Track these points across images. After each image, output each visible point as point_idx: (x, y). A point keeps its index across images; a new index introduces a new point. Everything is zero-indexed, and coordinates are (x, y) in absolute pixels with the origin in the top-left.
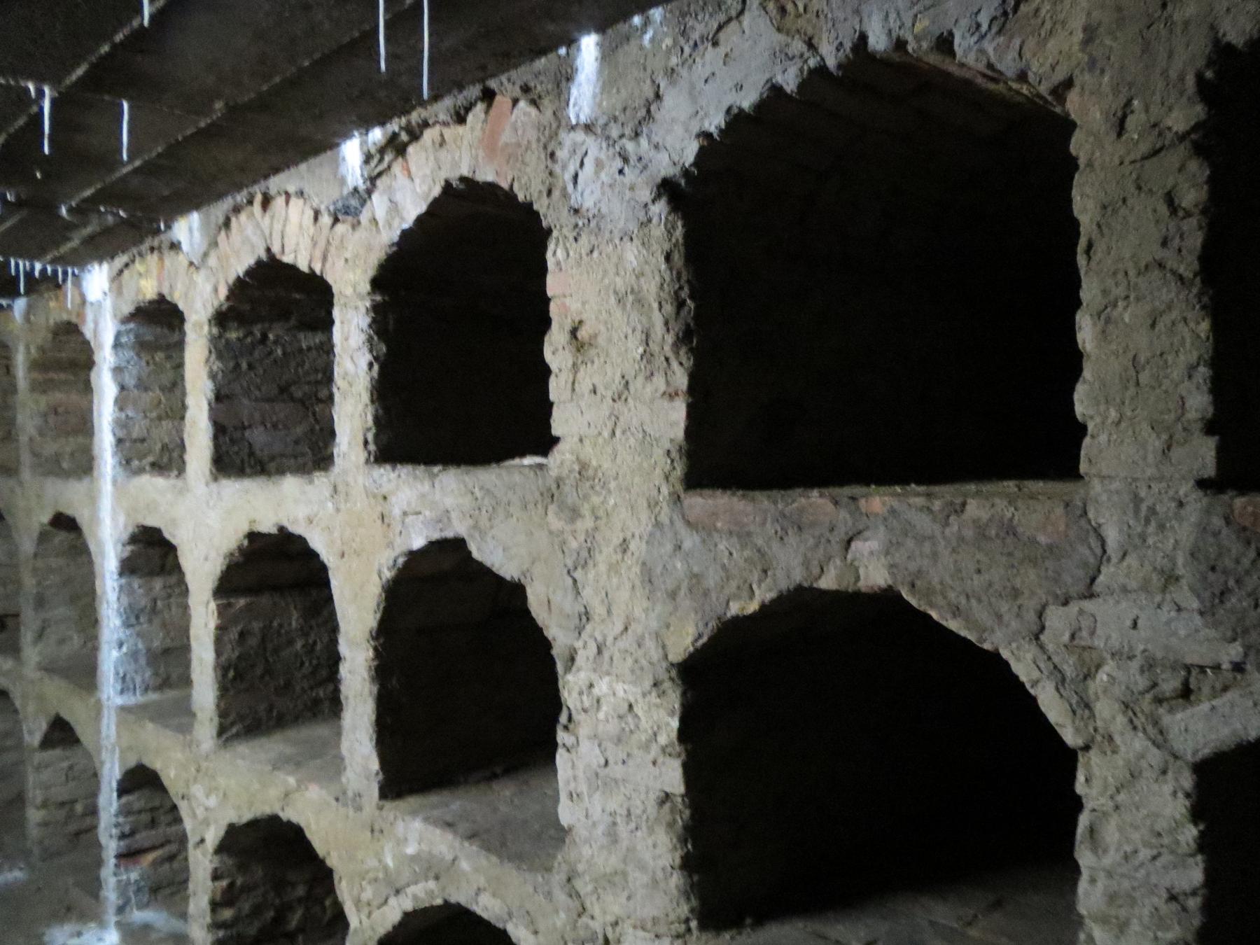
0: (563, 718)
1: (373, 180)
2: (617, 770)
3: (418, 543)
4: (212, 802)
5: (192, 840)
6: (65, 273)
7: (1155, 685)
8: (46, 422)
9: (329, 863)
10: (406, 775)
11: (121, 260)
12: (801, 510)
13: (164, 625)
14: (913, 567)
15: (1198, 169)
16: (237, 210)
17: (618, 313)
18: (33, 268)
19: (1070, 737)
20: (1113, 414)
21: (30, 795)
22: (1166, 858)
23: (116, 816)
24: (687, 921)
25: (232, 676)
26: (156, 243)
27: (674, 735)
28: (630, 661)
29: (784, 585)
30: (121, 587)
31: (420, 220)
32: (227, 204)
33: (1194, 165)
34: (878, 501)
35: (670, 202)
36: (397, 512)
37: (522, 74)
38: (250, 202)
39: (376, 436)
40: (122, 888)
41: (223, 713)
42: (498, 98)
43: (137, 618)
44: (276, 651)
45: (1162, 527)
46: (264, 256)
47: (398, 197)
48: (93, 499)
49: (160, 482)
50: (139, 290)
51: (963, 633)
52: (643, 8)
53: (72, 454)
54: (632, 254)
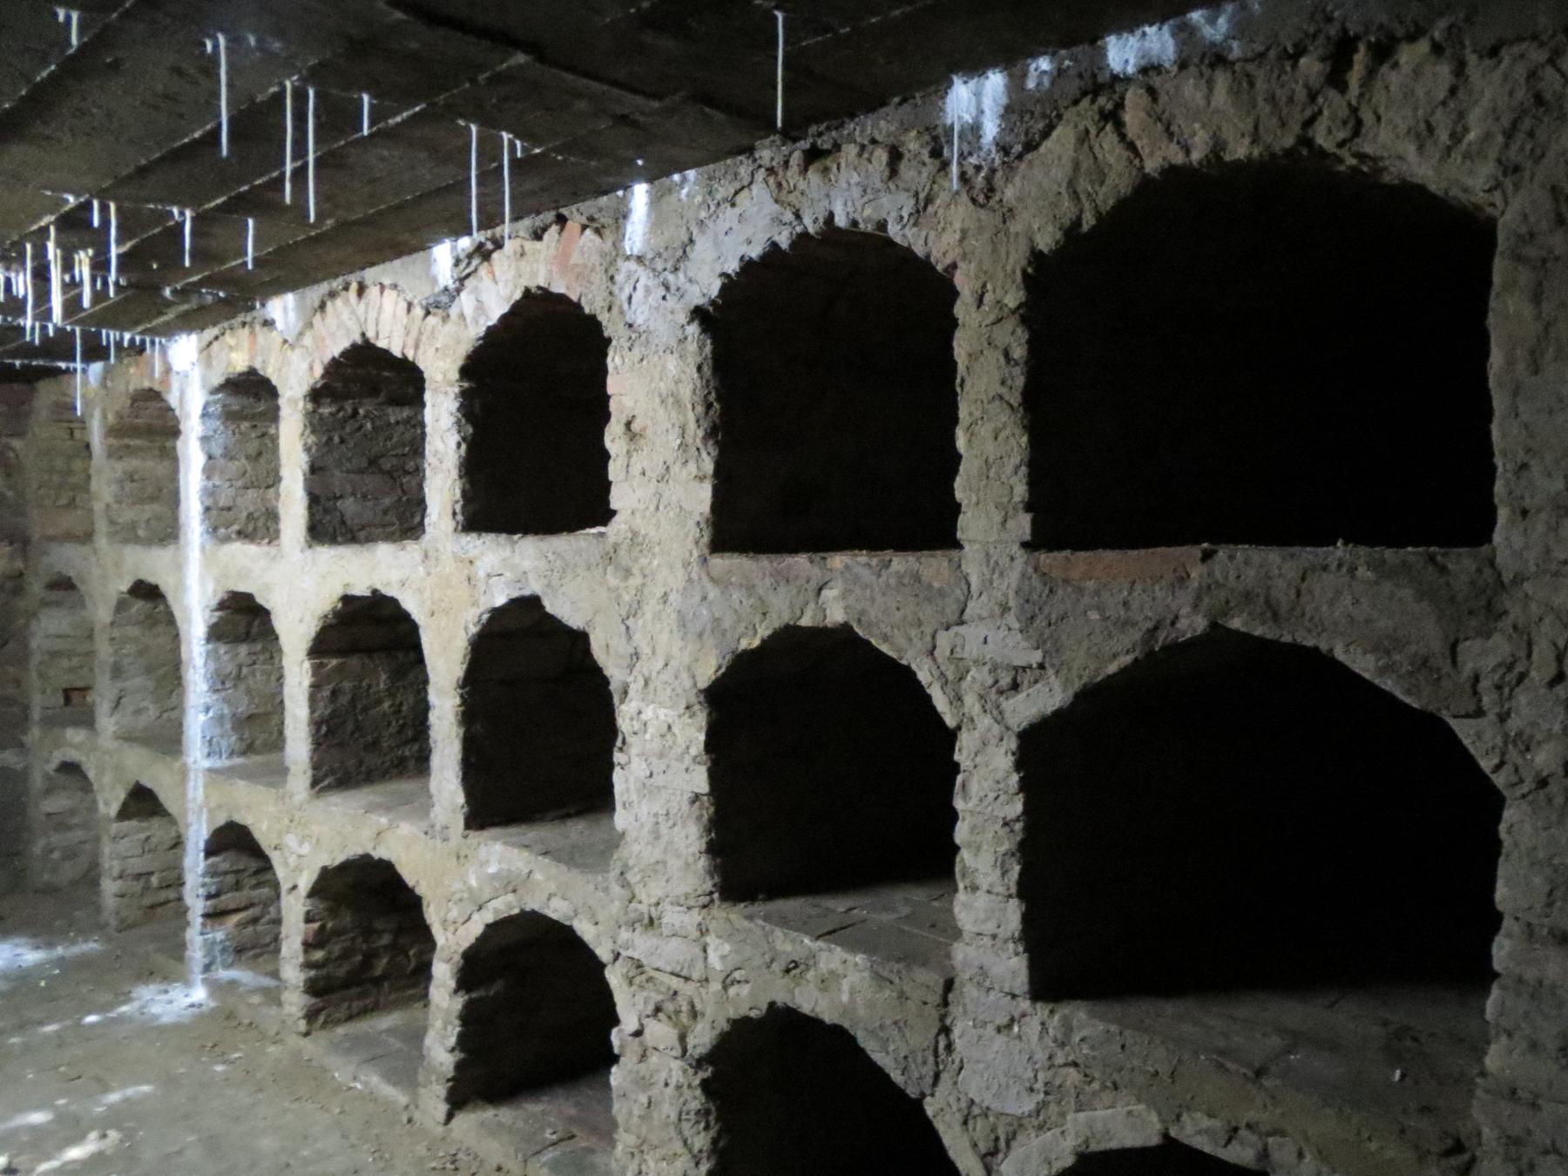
0: (619, 743)
1: (462, 280)
2: (659, 780)
3: (500, 600)
4: (306, 849)
5: (285, 887)
6: (153, 343)
7: (996, 682)
8: (122, 488)
9: (418, 891)
10: (490, 806)
11: (211, 332)
12: (790, 567)
13: (249, 691)
14: (859, 607)
15: (1022, 334)
16: (333, 295)
17: (661, 411)
18: (122, 338)
19: (950, 721)
20: (974, 499)
21: (107, 865)
22: (1002, 798)
23: (204, 876)
24: (711, 893)
25: (326, 732)
26: (248, 319)
27: (702, 746)
28: (669, 690)
29: (777, 624)
30: (208, 653)
31: (504, 318)
32: (324, 288)
33: (1019, 331)
34: (838, 560)
35: (701, 324)
36: (481, 574)
37: (589, 207)
38: (346, 288)
39: (464, 507)
40: (209, 946)
41: (316, 766)
42: (569, 223)
44: (365, 710)
45: (1001, 574)
46: (359, 341)
47: (484, 297)
48: (179, 567)
49: (252, 549)
50: (229, 363)
51: (890, 653)
52: (681, 170)
53: (148, 521)
54: (672, 364)
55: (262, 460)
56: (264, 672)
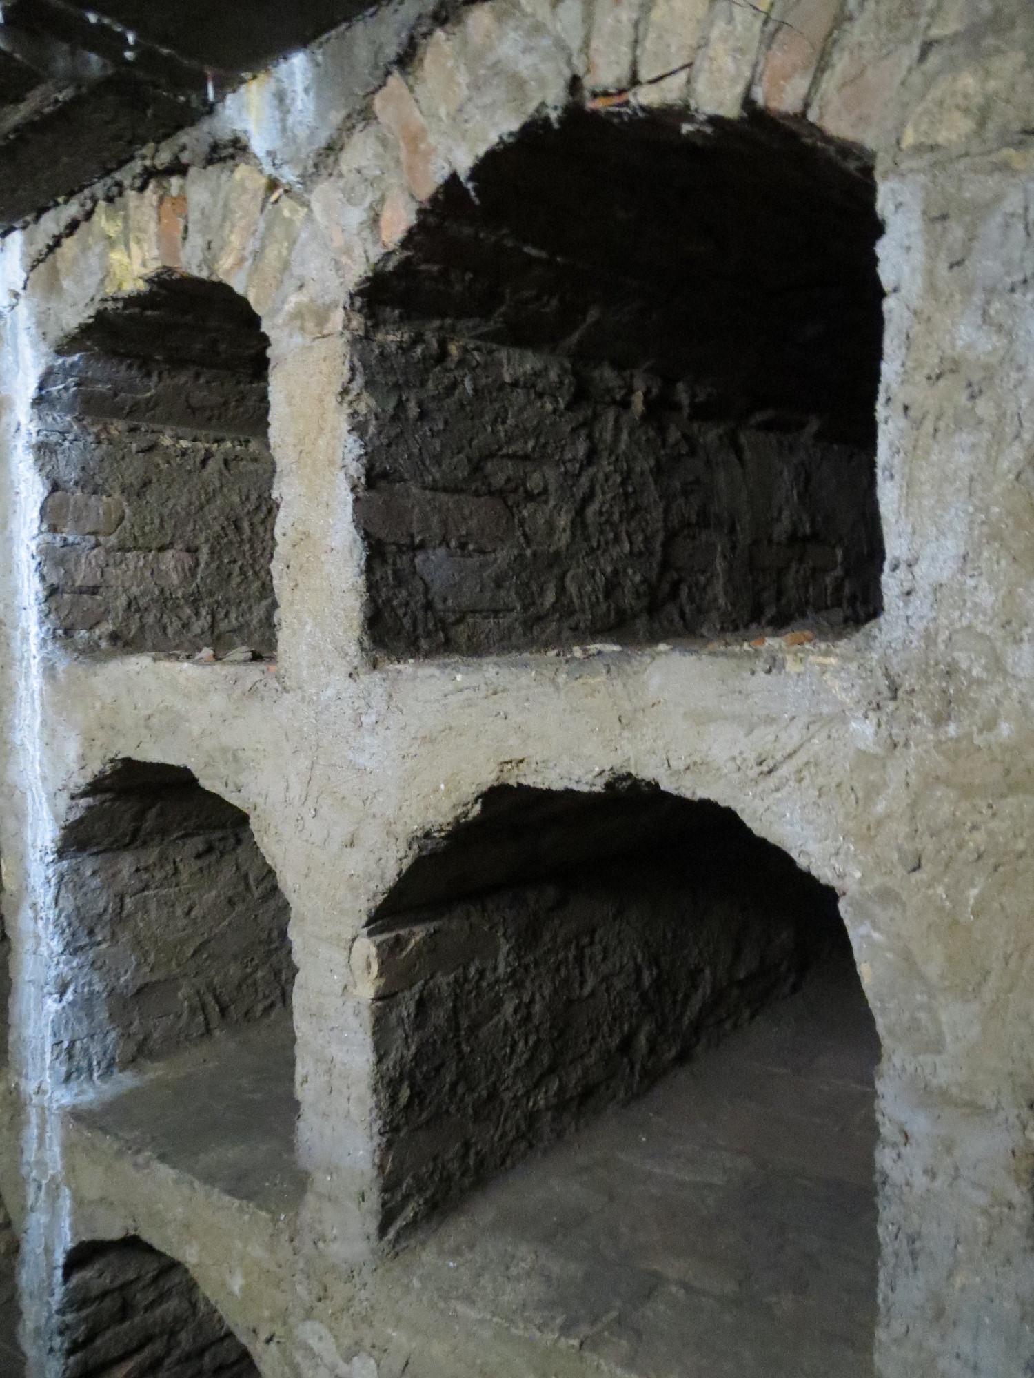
43: (91, 932)
44: (475, 1027)
50: (107, 273)
55: (151, 496)
56: (163, 903)
